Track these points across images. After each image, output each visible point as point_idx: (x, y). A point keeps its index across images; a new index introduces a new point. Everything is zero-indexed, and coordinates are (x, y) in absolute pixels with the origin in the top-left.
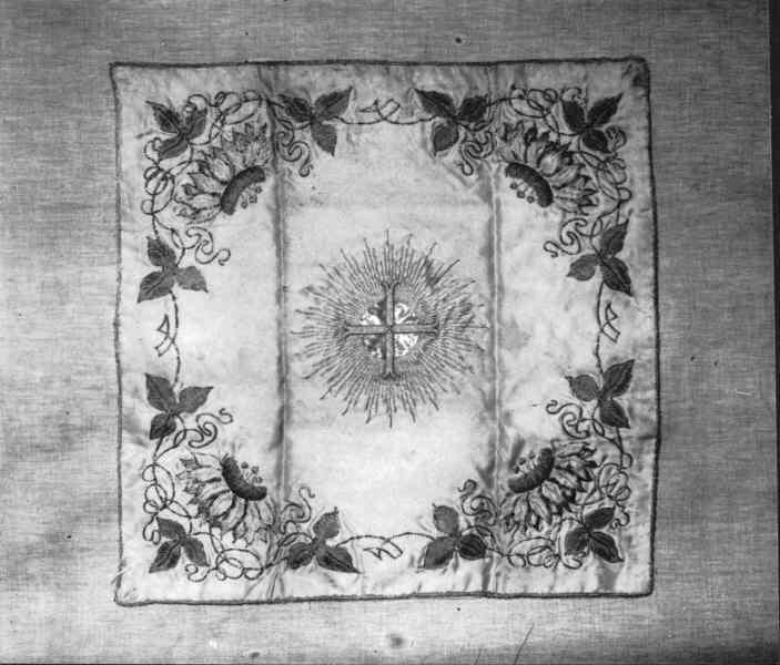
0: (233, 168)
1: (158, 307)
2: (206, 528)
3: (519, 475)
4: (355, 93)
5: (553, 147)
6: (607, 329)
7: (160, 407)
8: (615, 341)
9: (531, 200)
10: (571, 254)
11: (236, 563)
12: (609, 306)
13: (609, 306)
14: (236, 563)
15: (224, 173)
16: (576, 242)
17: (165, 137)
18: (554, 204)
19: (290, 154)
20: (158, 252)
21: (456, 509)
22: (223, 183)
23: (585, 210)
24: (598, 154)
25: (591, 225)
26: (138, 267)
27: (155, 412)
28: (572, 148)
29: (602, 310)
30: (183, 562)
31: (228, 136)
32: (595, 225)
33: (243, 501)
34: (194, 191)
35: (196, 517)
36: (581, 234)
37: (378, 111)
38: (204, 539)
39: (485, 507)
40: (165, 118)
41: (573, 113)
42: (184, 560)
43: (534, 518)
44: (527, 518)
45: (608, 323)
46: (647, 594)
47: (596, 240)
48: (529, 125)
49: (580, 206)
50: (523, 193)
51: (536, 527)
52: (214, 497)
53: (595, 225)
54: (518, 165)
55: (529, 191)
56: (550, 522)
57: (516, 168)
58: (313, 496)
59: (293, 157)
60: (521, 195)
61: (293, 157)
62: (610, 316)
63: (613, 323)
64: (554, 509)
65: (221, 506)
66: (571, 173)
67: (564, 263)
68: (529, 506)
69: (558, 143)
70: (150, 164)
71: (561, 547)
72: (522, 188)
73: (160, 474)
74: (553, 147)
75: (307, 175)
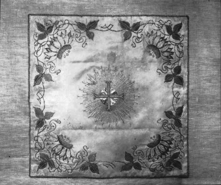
0: (59, 145)
1: (117, 27)
2: (50, 40)
3: (155, 55)
4: (35, 106)
5: (52, 43)
6: (109, 28)
7: (132, 167)
8: (113, 26)
9: (69, 52)
10: (86, 39)
11: (39, 49)
12: (102, 27)
13: (102, 27)
14: (39, 49)
15: (160, 45)
16: (82, 38)
17: (48, 166)
18: (71, 44)
19: (54, 126)
20: (136, 26)
21: (166, 75)
22: (157, 44)
23: (72, 34)
24: (53, 29)
25: (77, 33)
26: (131, 21)
27: (133, 168)
28: (52, 37)
29: (103, 29)
30: (178, 159)
31: (171, 46)
32: (77, 32)
33: (161, 142)
34: (65, 157)
35: (166, 155)
36: (80, 36)
37: (40, 99)
38: (46, 40)
39: (52, 128)
40: (42, 166)
41: (41, 37)
42: (178, 159)
43: (169, 50)
44: (168, 52)
45: (107, 27)
46: (188, 18)
47: (82, 31)
48: (45, 51)
49: (71, 36)
50: (67, 54)
51: (171, 49)
52: (160, 150)
53: (77, 32)
54: (58, 55)
55: (66, 52)
56: (170, 45)
57: (59, 56)
58: (161, 119)
59: (54, 125)
60: (67, 55)
61: (54, 125)
62: (105, 27)
63: (107, 26)
64: (166, 44)
65: (163, 149)
66: (59, 38)
67: (89, 41)
68: (165, 52)
69: (50, 42)
70: (56, 170)
71: (178, 42)
72: (65, 54)
73: (67, 25)
74: (52, 43)
75: (61, 122)
